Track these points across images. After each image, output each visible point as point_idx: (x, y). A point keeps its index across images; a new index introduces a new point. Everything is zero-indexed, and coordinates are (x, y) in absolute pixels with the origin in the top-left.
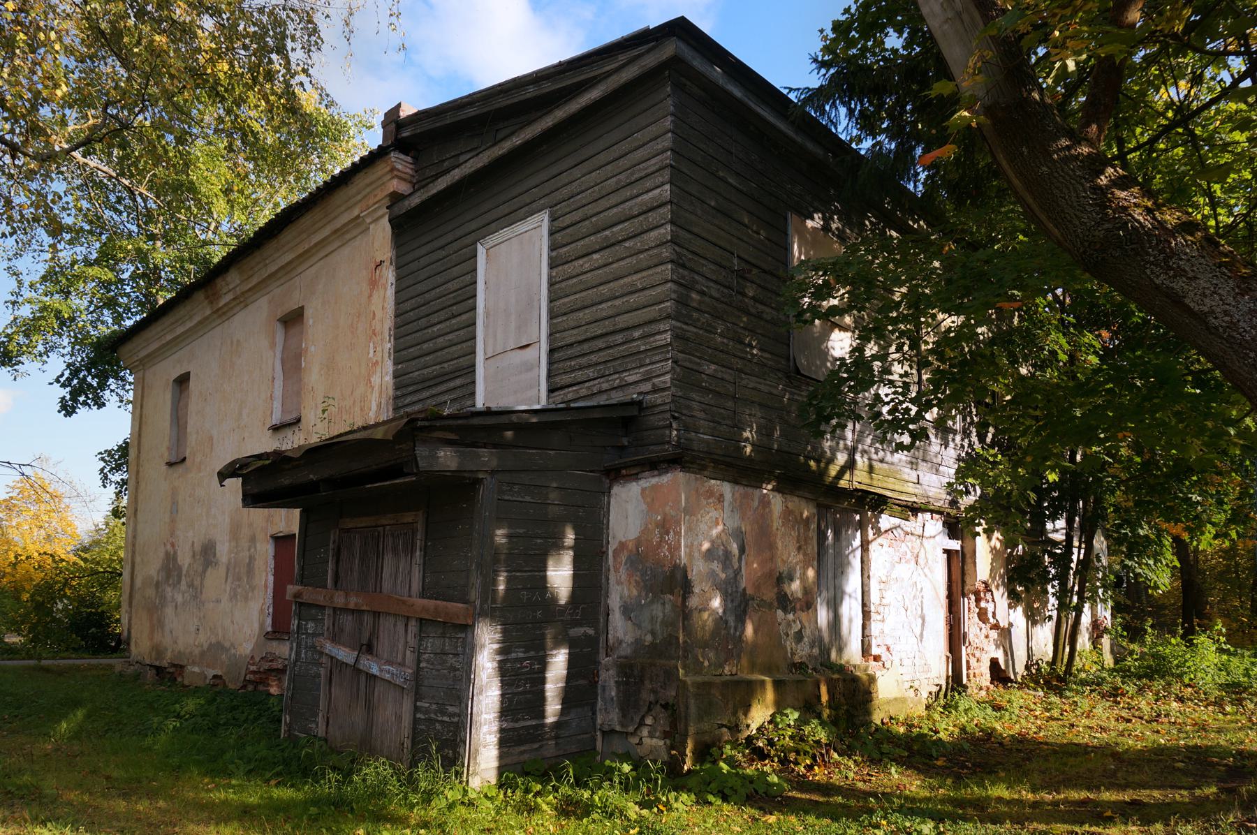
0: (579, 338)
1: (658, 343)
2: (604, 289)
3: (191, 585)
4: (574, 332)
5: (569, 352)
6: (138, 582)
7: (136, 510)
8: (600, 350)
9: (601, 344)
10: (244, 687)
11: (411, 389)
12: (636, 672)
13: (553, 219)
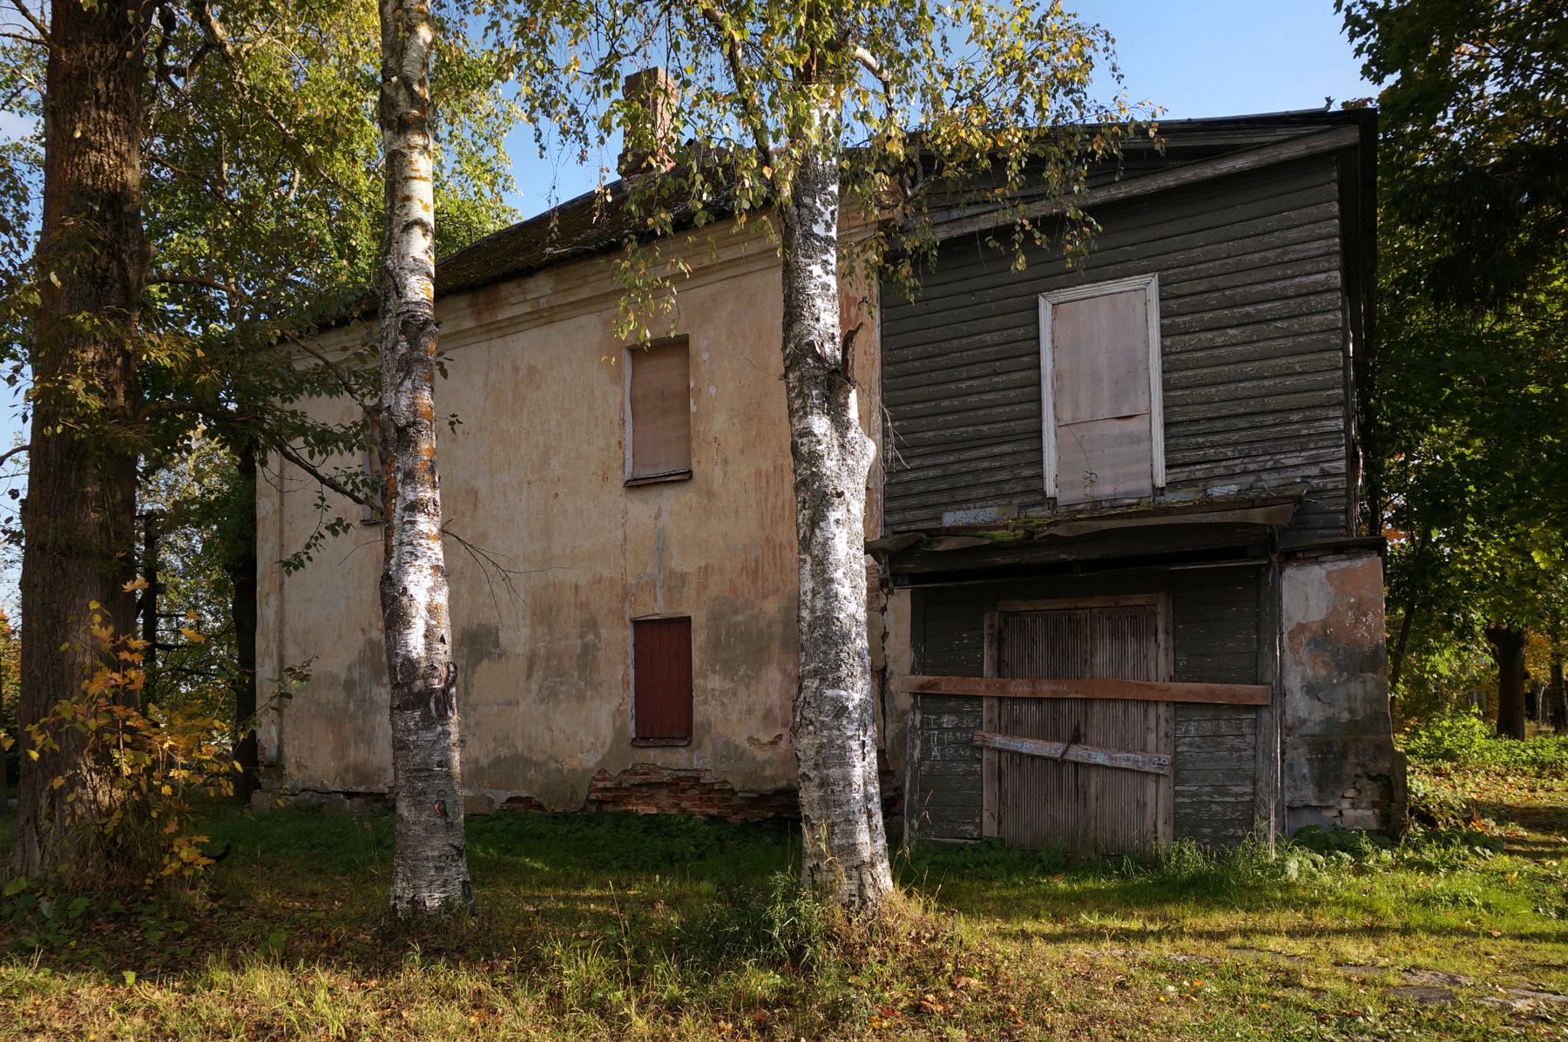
2: (1248, 368)
4: (1205, 407)
9: (1243, 423)
13: (1163, 284)
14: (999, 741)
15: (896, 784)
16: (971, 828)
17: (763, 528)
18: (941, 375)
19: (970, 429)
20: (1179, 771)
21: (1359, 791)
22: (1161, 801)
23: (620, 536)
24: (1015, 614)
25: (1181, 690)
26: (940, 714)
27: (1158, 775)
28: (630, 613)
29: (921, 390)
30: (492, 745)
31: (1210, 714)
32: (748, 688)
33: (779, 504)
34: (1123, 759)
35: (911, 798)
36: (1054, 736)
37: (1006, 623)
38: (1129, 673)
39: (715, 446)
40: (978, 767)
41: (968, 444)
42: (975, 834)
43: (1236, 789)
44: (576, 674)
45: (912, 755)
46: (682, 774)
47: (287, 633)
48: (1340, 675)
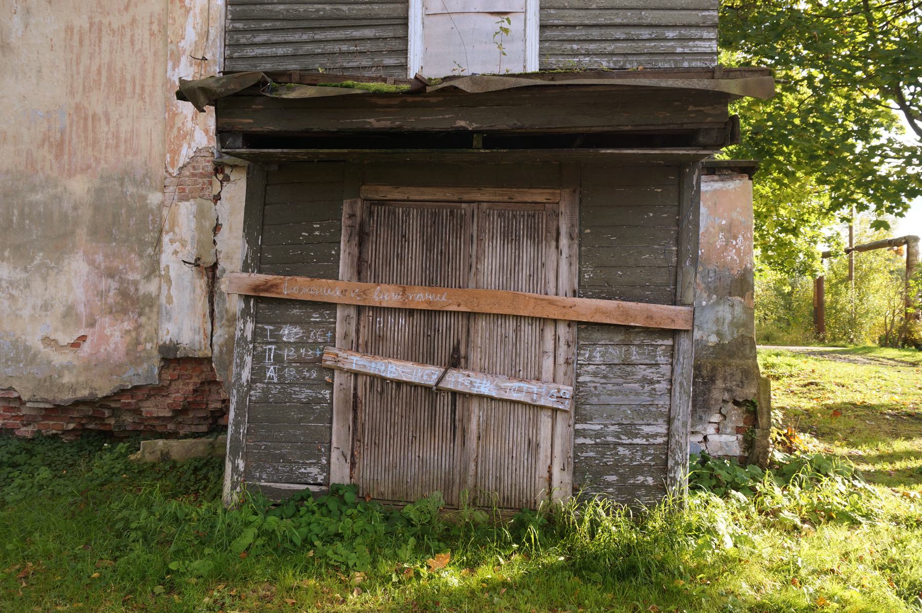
0: (587, 22)
1: (700, 50)
5: (569, 33)
8: (618, 40)
9: (619, 34)
11: (265, 24)
12: (704, 373)
14: (357, 361)
15: (223, 396)
16: (314, 470)
17: (72, 93)
19: (328, 7)
20: (580, 408)
21: (725, 417)
22: (558, 442)
24: (382, 202)
25: (591, 308)
27: (555, 410)
31: (618, 338)
32: (44, 279)
33: (94, 68)
34: (515, 390)
35: (237, 431)
36: (428, 359)
37: (371, 214)
38: (523, 283)
41: (324, 23)
42: (320, 479)
43: (647, 429)
45: (239, 375)
48: (709, 297)
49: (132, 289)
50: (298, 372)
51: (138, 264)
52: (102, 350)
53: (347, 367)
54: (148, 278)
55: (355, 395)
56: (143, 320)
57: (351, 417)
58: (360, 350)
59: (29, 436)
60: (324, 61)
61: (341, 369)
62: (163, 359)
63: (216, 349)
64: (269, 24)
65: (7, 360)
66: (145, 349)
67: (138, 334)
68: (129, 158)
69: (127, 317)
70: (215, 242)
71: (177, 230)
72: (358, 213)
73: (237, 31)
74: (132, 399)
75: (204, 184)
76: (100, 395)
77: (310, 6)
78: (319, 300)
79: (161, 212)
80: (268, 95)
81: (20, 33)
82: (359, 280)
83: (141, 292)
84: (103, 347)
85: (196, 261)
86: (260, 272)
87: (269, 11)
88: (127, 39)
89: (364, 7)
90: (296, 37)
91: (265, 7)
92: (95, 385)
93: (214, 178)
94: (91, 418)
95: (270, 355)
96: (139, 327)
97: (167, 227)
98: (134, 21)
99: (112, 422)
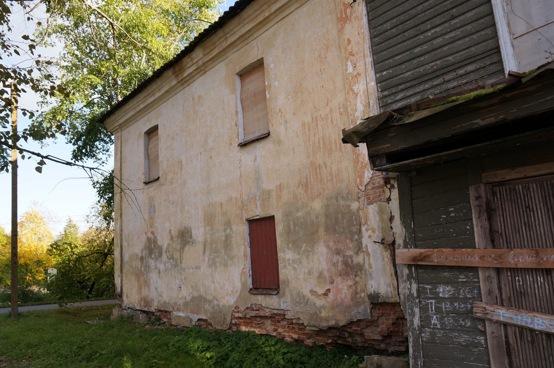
3: (171, 258)
6: (126, 257)
7: (121, 214)
10: (230, 328)
11: (401, 87)
14: (503, 314)
17: (308, 157)
18: (412, 32)
19: (438, 62)
23: (239, 174)
24: (502, 183)
26: (435, 284)
28: (246, 216)
29: (399, 46)
30: (191, 290)
32: (307, 258)
33: (317, 141)
37: (494, 194)
39: (280, 114)
40: (482, 339)
41: (438, 73)
44: (223, 252)
46: (276, 312)
47: (123, 236)
49: (350, 260)
50: (455, 321)
51: (351, 245)
52: (339, 297)
53: (495, 318)
54: (357, 253)
55: (507, 343)
56: (358, 279)
57: (506, 362)
58: (505, 304)
59: (311, 345)
60: (431, 91)
61: (491, 321)
62: (372, 303)
63: (402, 296)
64: (403, 87)
65: (296, 303)
66: (361, 297)
67: (356, 288)
68: (339, 185)
69: (349, 278)
70: (391, 228)
71: (369, 223)
72: (483, 195)
73: (385, 97)
74: (358, 327)
75: (380, 192)
76: (341, 324)
77: (427, 66)
78: (462, 265)
79: (359, 213)
80: (396, 124)
81: (284, 133)
82: (494, 247)
83: (355, 262)
84: (339, 295)
85: (382, 240)
86: (416, 247)
87: (401, 78)
88: (329, 121)
89: (464, 52)
90: (422, 88)
91: (399, 77)
92: (338, 318)
93: (385, 187)
94: (339, 337)
95: (432, 308)
96: (356, 283)
97: (363, 222)
98: (331, 110)
99: (350, 340)
